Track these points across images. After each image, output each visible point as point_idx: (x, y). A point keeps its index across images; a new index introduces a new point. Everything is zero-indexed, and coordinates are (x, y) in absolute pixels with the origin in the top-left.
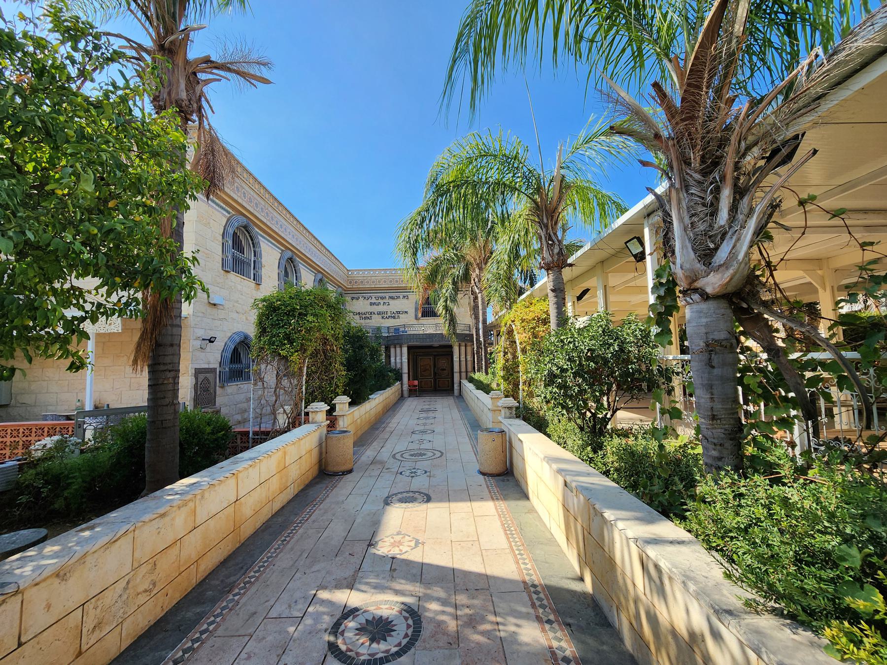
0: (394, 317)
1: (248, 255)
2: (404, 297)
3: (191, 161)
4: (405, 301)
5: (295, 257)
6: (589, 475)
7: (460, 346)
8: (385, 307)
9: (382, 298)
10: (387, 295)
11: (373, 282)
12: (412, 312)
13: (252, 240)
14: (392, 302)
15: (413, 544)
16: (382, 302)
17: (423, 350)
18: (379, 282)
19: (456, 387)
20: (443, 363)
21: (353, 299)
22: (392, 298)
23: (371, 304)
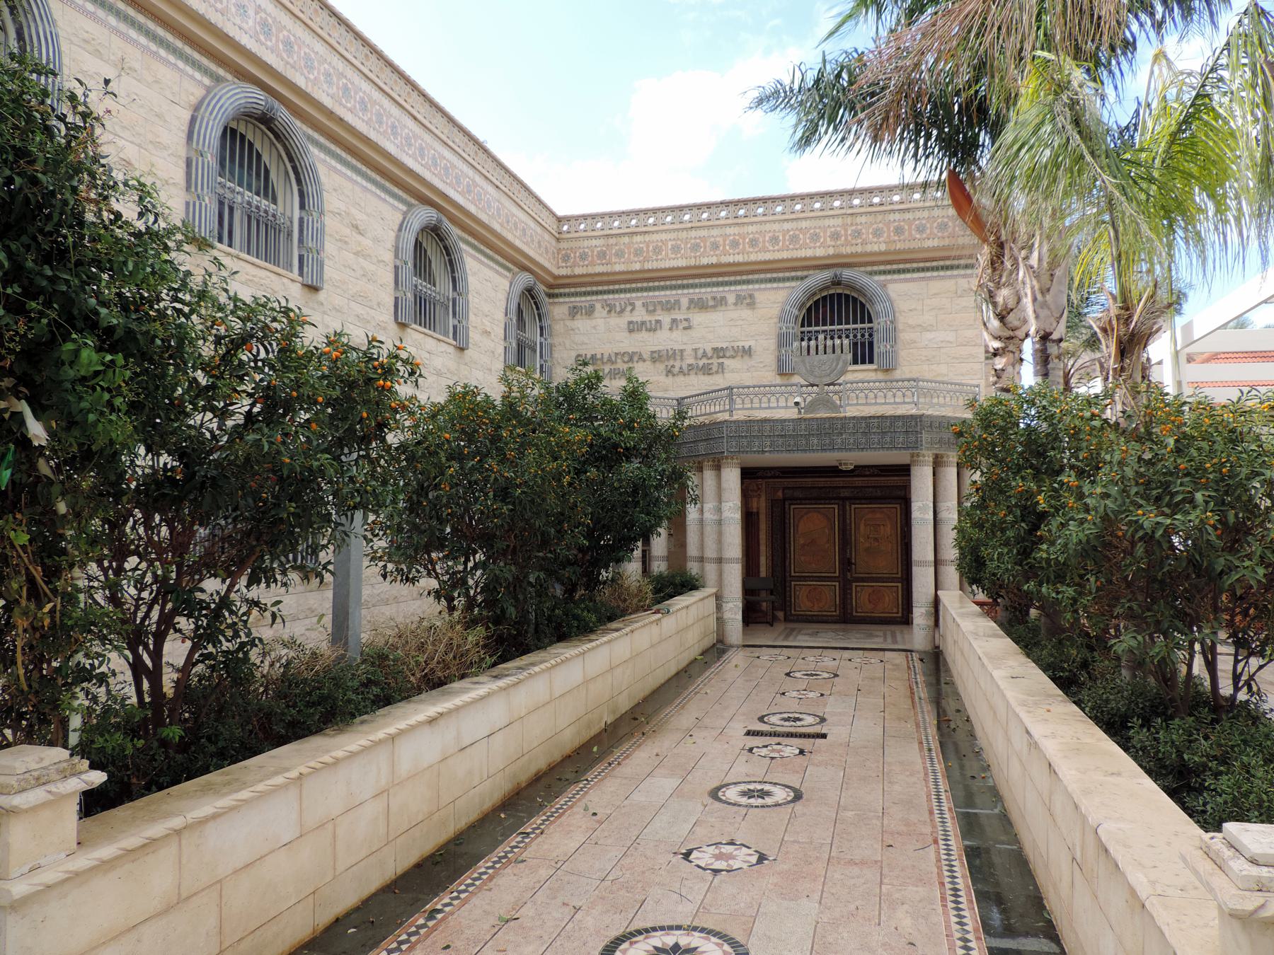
0: (706, 370)
1: (287, 207)
2: (739, 299)
3: (1231, 863)
4: (746, 313)
5: (446, 224)
6: (309, 138)
7: (938, 463)
8: (677, 335)
9: (670, 307)
10: (684, 296)
11: (638, 252)
12: (766, 349)
13: (291, 160)
14: (698, 318)
15: (754, 859)
16: (666, 319)
17: (808, 481)
18: (657, 250)
19: (920, 614)
20: (870, 523)
21: (574, 312)
22: (700, 305)
23: (633, 328)
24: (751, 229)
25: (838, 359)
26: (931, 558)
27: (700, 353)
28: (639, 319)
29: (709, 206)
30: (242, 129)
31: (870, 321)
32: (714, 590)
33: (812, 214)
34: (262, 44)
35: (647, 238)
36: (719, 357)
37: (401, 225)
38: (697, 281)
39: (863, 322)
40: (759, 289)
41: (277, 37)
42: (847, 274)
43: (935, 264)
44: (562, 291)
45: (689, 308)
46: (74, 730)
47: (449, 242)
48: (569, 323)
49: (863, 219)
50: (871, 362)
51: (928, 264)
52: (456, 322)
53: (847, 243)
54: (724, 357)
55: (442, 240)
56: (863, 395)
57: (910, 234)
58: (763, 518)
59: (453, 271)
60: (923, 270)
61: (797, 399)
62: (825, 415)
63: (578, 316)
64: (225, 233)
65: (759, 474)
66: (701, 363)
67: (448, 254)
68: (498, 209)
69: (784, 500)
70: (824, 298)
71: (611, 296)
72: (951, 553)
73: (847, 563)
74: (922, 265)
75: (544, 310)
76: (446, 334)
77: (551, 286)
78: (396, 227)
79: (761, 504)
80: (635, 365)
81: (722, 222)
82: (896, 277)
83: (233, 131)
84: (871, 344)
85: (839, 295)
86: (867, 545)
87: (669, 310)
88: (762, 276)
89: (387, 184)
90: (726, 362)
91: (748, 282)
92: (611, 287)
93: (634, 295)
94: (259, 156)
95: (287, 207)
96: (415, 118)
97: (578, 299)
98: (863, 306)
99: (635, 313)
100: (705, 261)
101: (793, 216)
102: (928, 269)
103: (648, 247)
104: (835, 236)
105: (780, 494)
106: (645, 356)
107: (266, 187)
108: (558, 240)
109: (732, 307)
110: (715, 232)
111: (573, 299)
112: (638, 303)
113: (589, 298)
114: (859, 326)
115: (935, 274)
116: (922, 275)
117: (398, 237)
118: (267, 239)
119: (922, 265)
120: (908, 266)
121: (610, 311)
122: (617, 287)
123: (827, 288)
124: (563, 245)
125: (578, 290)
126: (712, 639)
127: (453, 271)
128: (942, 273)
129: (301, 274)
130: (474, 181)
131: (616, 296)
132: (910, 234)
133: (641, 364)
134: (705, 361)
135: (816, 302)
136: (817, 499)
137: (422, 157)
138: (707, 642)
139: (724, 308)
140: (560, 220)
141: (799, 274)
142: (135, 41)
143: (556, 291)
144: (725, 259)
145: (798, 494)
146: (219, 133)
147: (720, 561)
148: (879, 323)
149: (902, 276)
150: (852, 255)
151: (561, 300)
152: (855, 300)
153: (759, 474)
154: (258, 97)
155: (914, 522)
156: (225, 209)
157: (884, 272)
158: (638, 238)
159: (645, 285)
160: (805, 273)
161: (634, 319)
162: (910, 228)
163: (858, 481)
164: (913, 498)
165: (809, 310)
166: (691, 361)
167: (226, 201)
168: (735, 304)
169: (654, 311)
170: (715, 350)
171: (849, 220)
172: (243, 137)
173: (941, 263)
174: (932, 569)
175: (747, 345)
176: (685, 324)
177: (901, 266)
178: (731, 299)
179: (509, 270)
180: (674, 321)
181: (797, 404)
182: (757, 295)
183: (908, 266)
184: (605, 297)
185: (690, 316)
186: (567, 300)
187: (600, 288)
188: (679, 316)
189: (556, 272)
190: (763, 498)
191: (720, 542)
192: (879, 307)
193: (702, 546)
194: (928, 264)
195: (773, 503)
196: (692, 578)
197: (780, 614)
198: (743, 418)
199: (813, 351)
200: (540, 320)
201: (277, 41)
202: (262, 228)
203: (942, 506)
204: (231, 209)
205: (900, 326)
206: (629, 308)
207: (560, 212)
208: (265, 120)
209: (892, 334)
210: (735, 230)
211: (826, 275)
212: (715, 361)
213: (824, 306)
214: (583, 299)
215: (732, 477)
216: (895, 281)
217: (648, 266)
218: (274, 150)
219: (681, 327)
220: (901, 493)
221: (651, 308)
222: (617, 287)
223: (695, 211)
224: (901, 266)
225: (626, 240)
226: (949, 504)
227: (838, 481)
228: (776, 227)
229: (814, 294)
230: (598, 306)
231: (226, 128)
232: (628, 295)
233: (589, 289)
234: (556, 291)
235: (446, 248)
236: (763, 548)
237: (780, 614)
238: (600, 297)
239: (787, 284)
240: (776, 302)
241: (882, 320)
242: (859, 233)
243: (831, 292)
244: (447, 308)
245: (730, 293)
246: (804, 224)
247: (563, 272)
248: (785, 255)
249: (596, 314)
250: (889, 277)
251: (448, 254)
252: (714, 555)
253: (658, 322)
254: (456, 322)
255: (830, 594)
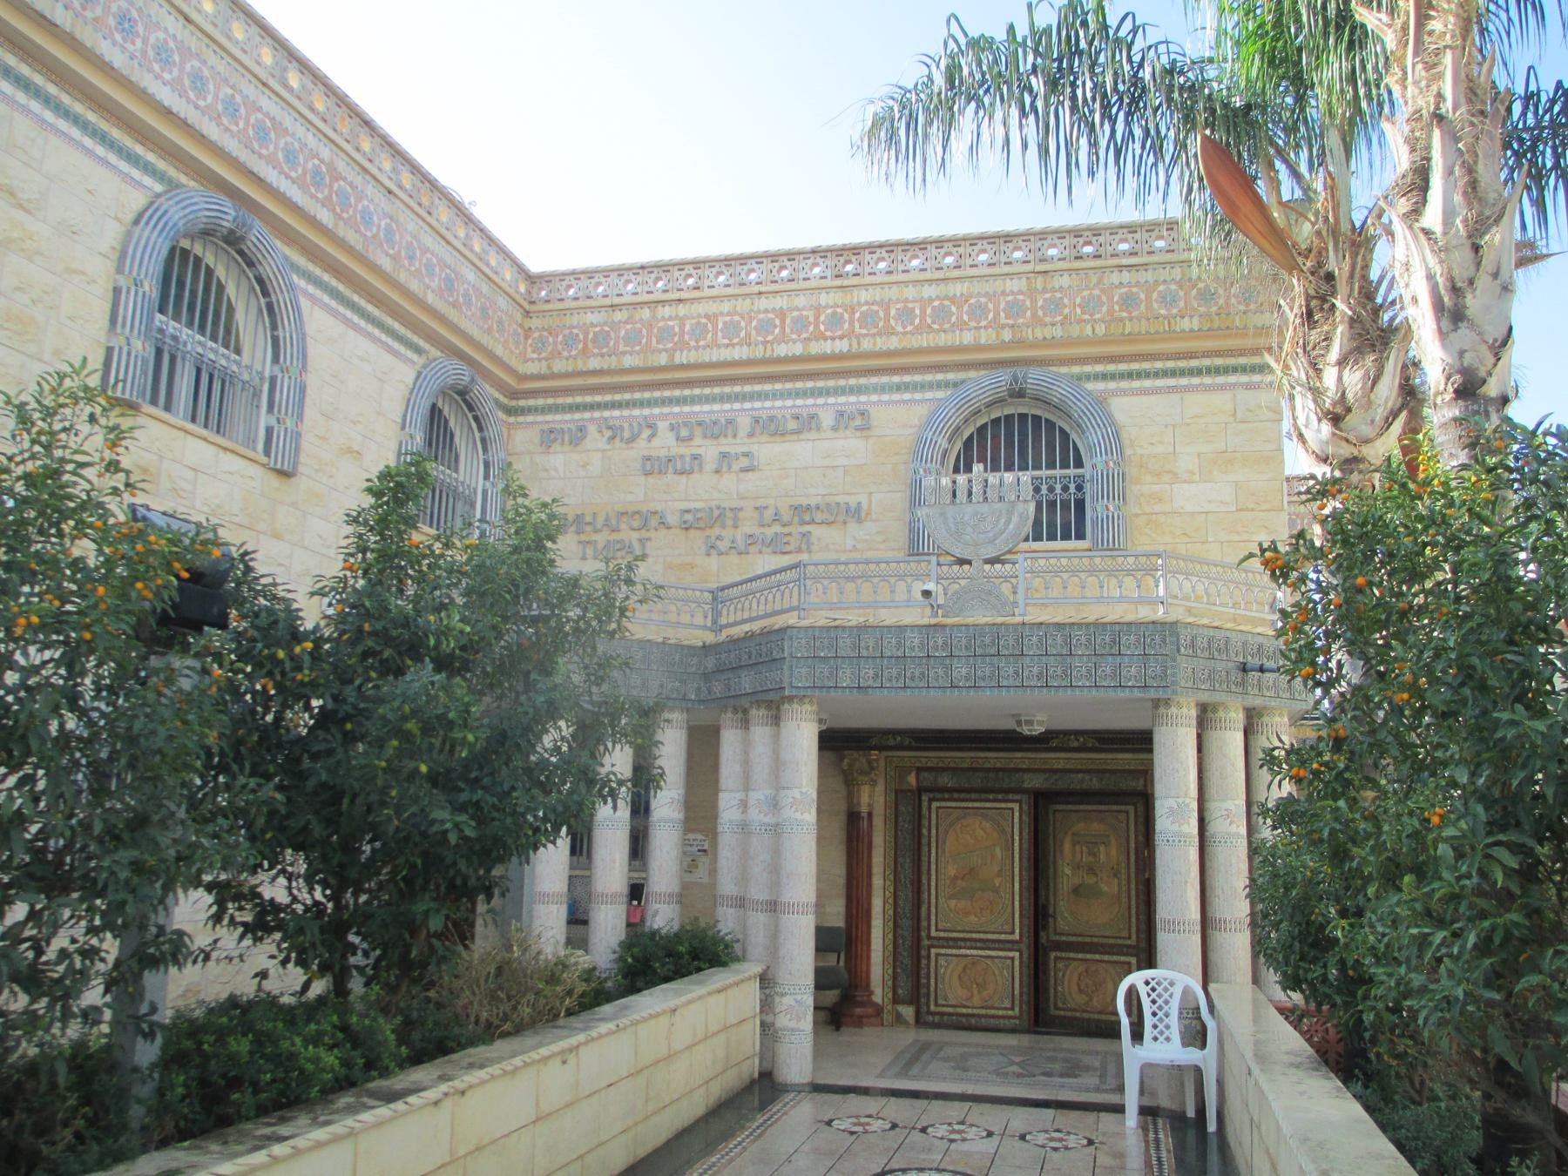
7: (1205, 718)
8: (729, 481)
9: (718, 429)
10: (743, 413)
14: (767, 451)
16: (711, 452)
17: (964, 758)
21: (550, 437)
22: (770, 428)
23: (653, 467)
24: (864, 295)
25: (1010, 513)
26: (1195, 914)
27: (769, 515)
28: (663, 453)
29: (791, 255)
30: (198, 249)
31: (1079, 463)
32: (758, 969)
33: (974, 272)
34: (228, 130)
35: (682, 310)
36: (803, 523)
37: (141, 215)
38: (768, 387)
39: (1065, 465)
40: (879, 402)
41: (182, 70)
42: (1034, 377)
43: (1194, 363)
44: (531, 402)
45: (751, 435)
46: (139, 1101)
47: (267, 270)
48: (538, 459)
49: (1065, 281)
50: (1081, 536)
51: (1182, 364)
52: (273, 422)
53: (1037, 321)
54: (812, 522)
55: (251, 264)
56: (1059, 590)
57: (1149, 308)
58: (878, 822)
59: (274, 327)
60: (1173, 373)
61: (930, 586)
62: (983, 620)
63: (557, 447)
64: (160, 393)
65: (874, 742)
66: (769, 532)
67: (266, 293)
68: (389, 231)
69: (920, 790)
70: (996, 422)
71: (616, 413)
72: (1235, 904)
73: (1039, 914)
74: (1170, 364)
75: (491, 432)
76: (251, 442)
77: (514, 395)
78: (130, 217)
79: (874, 798)
80: (652, 534)
81: (813, 283)
82: (1124, 384)
83: (185, 253)
84: (1080, 505)
85: (1023, 417)
86: (1077, 881)
87: (715, 437)
88: (885, 379)
89: (116, 134)
90: (817, 531)
91: (860, 390)
92: (618, 397)
93: (656, 411)
94: (446, 421)
95: (253, 355)
96: (448, 243)
97: (558, 417)
98: (1065, 435)
99: (656, 442)
100: (782, 350)
101: (940, 275)
102: (1182, 373)
103: (682, 326)
104: (1014, 310)
105: (912, 779)
106: (672, 519)
107: (228, 331)
108: (527, 314)
109: (830, 434)
110: (801, 301)
111: (549, 418)
112: (662, 426)
113: (577, 416)
114: (1058, 472)
115: (1196, 381)
116: (1172, 382)
117: (129, 234)
118: (212, 402)
119: (1170, 364)
120: (1146, 365)
121: (613, 438)
122: (627, 396)
123: (1000, 401)
124: (535, 323)
125: (560, 401)
126: (753, 1068)
127: (274, 327)
128: (1208, 380)
129: (267, 452)
130: (331, 167)
131: (626, 413)
132: (1149, 308)
133: (663, 532)
134: (777, 528)
135: (981, 430)
136: (983, 792)
137: (201, 93)
138: (732, 1080)
139: (813, 435)
140: (532, 279)
141: (951, 376)
142: (114, 167)
143: (522, 403)
144: (815, 348)
145: (945, 780)
146: (165, 252)
147: (773, 907)
148: (1095, 464)
149: (1136, 384)
150: (1046, 343)
151: (530, 419)
152: (1051, 425)
153: (874, 742)
154: (229, 214)
155: (1159, 839)
156: (164, 357)
157: (1104, 377)
158: (667, 311)
159: (677, 393)
160: (962, 375)
161: (654, 453)
162: (1148, 298)
163: (1058, 759)
164: (1159, 789)
165: (968, 443)
166: (755, 530)
167: (166, 348)
168: (834, 429)
169: (690, 438)
170: (796, 508)
171: (1039, 282)
172: (198, 260)
173: (1207, 362)
174: (1197, 938)
175: (853, 501)
176: (744, 462)
177: (1135, 366)
178: (827, 419)
179: (418, 350)
180: (724, 455)
181: (927, 594)
182: (873, 412)
183: (1146, 365)
184: (606, 414)
185: (754, 448)
186: (540, 418)
187: (598, 398)
188: (727, 445)
189: (523, 369)
190: (880, 788)
191: (775, 868)
192: (1094, 436)
193: (744, 878)
194: (1182, 364)
195: (900, 795)
196: (717, 940)
197: (908, 1012)
198: (823, 622)
199: (962, 495)
200: (485, 450)
201: (331, 186)
202: (217, 386)
203: (1215, 809)
204: (211, 377)
205: (1132, 471)
206: (646, 433)
207: (535, 267)
208: (233, 240)
209: (1117, 487)
210: (837, 297)
211: (1003, 377)
212: (795, 529)
213: (995, 438)
214: (568, 417)
215: (801, 736)
216: (1124, 393)
217: (681, 358)
218: (243, 279)
219: (735, 467)
220: (1137, 784)
221: (684, 433)
222: (627, 396)
223: (767, 265)
224: (1135, 366)
225: (646, 313)
226: (1230, 805)
227: (1020, 758)
228: (910, 292)
229: (977, 412)
230: (592, 428)
231: (173, 250)
232: (646, 412)
233: (579, 399)
234: (522, 403)
235: (260, 281)
236: (877, 882)
237: (908, 1012)
238: (597, 414)
239: (929, 395)
240: (907, 416)
241: (1099, 461)
242: (1059, 304)
243: (1008, 411)
244: (257, 394)
245: (826, 409)
246: (958, 289)
247: (532, 368)
248: (923, 341)
249: (588, 443)
250: (1112, 385)
251: (266, 293)
252: (763, 896)
253: (695, 457)
254: (273, 422)
255: (1003, 977)
